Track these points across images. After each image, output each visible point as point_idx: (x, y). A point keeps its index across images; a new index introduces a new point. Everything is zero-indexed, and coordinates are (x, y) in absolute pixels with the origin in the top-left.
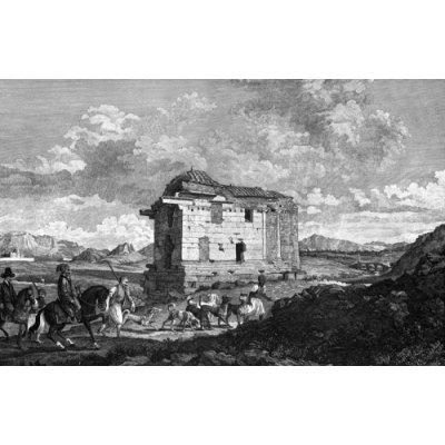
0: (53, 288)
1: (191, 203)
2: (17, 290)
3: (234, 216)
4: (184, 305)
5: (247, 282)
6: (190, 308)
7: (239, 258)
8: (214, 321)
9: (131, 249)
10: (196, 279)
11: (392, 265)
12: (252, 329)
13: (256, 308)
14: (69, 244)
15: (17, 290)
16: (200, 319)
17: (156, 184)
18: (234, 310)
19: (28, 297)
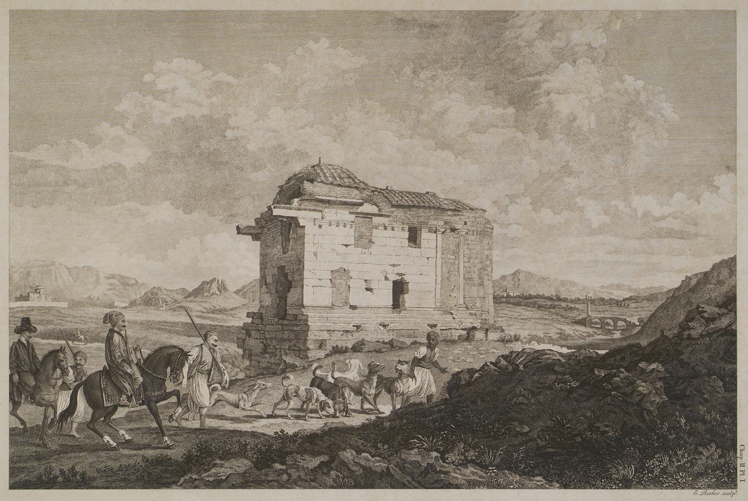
0: (99, 349)
1: (318, 215)
2: (40, 354)
3: (390, 238)
4: (308, 378)
5: (408, 341)
6: (317, 382)
7: (397, 305)
8: (354, 403)
9: (222, 288)
10: (325, 336)
11: (640, 320)
12: (414, 421)
13: (423, 385)
14: (124, 282)
15: (40, 354)
16: (333, 399)
17: (267, 179)
18: (388, 385)
19: (58, 364)
